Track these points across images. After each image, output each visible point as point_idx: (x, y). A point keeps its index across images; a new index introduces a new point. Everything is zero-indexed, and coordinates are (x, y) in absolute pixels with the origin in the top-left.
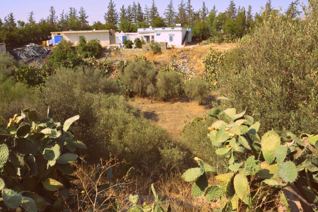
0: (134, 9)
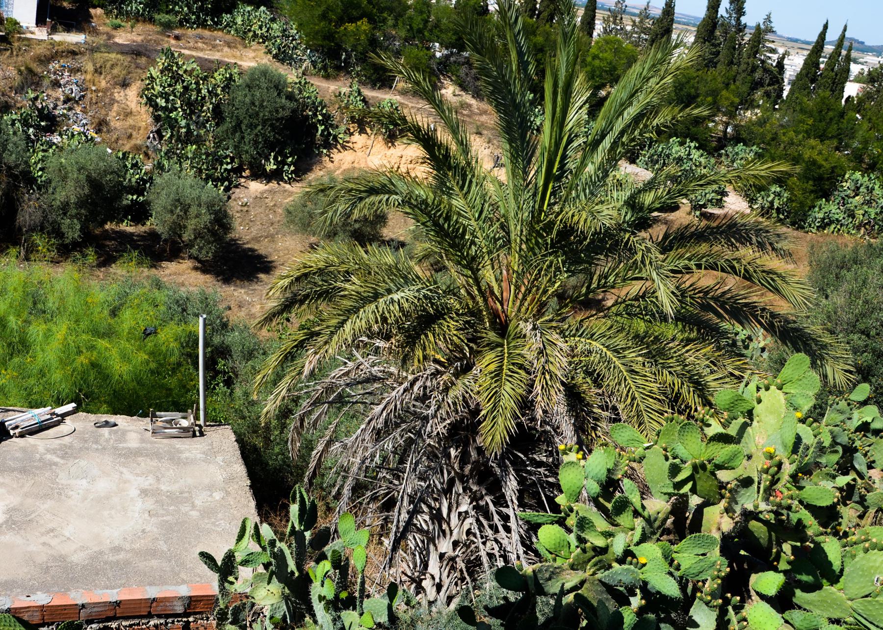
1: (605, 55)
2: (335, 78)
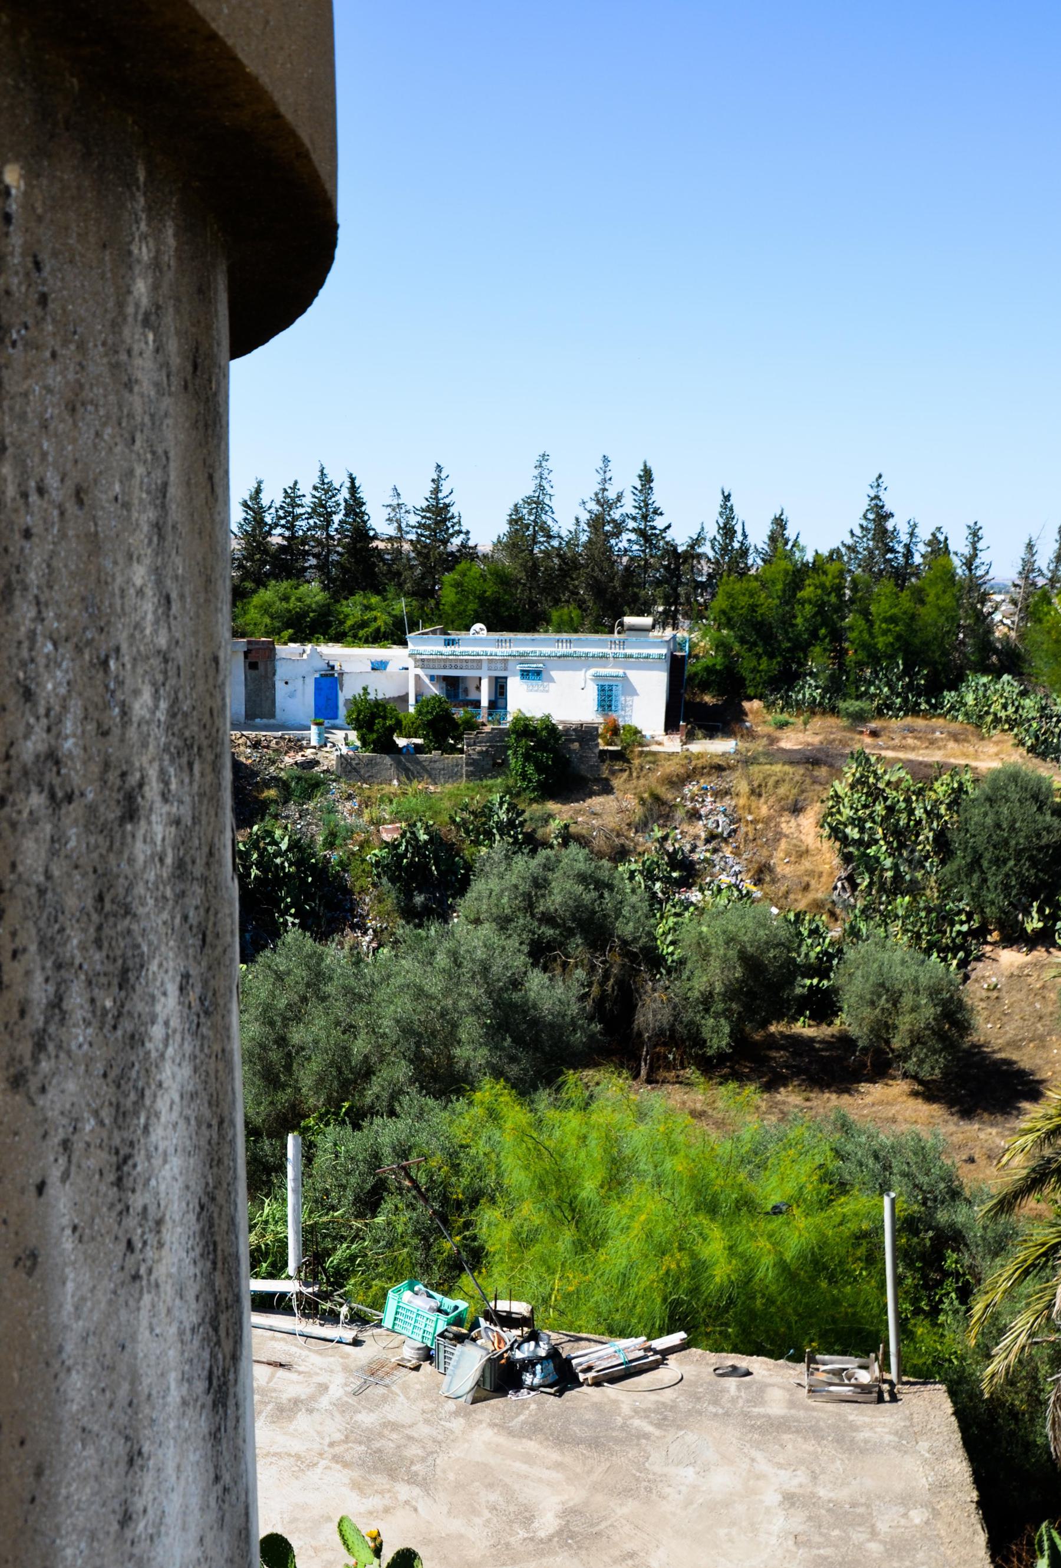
0: (322, 510)
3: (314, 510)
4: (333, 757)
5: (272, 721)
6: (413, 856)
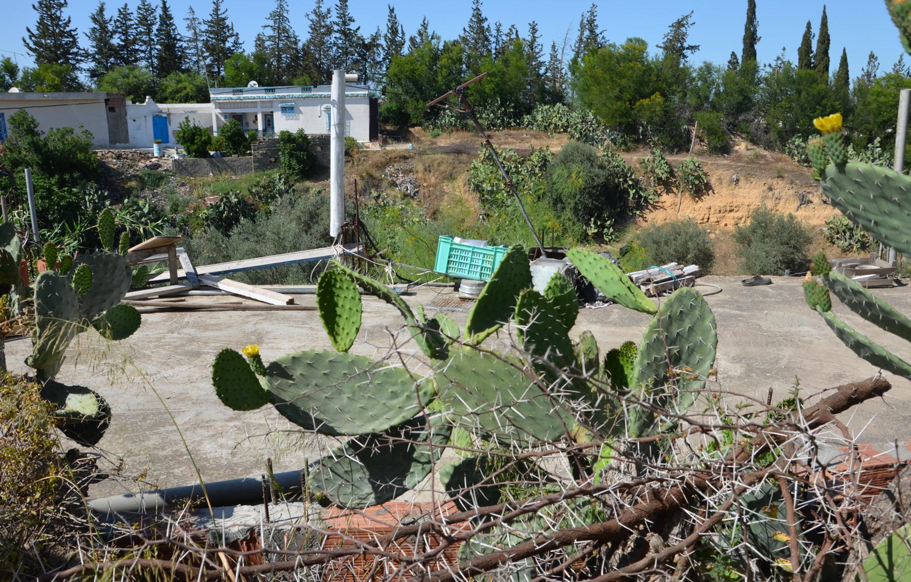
1: (889, 90)
2: (636, 150)
3: (140, 22)
4: (170, 161)
5: (127, 145)
6: (229, 213)
